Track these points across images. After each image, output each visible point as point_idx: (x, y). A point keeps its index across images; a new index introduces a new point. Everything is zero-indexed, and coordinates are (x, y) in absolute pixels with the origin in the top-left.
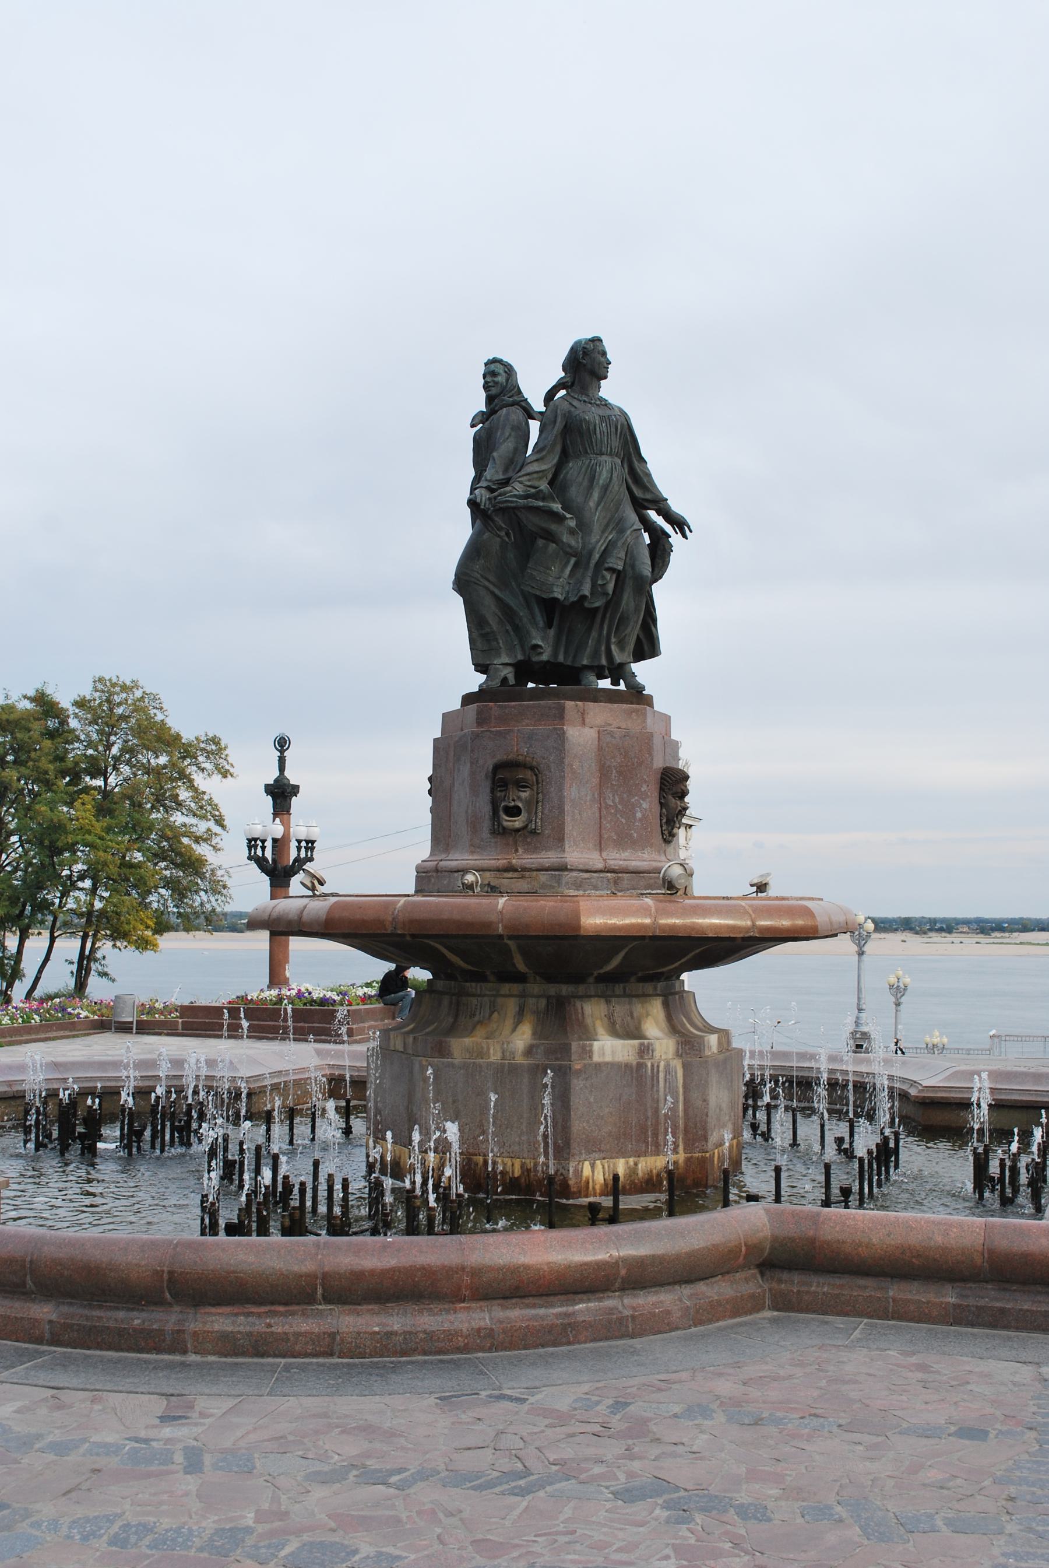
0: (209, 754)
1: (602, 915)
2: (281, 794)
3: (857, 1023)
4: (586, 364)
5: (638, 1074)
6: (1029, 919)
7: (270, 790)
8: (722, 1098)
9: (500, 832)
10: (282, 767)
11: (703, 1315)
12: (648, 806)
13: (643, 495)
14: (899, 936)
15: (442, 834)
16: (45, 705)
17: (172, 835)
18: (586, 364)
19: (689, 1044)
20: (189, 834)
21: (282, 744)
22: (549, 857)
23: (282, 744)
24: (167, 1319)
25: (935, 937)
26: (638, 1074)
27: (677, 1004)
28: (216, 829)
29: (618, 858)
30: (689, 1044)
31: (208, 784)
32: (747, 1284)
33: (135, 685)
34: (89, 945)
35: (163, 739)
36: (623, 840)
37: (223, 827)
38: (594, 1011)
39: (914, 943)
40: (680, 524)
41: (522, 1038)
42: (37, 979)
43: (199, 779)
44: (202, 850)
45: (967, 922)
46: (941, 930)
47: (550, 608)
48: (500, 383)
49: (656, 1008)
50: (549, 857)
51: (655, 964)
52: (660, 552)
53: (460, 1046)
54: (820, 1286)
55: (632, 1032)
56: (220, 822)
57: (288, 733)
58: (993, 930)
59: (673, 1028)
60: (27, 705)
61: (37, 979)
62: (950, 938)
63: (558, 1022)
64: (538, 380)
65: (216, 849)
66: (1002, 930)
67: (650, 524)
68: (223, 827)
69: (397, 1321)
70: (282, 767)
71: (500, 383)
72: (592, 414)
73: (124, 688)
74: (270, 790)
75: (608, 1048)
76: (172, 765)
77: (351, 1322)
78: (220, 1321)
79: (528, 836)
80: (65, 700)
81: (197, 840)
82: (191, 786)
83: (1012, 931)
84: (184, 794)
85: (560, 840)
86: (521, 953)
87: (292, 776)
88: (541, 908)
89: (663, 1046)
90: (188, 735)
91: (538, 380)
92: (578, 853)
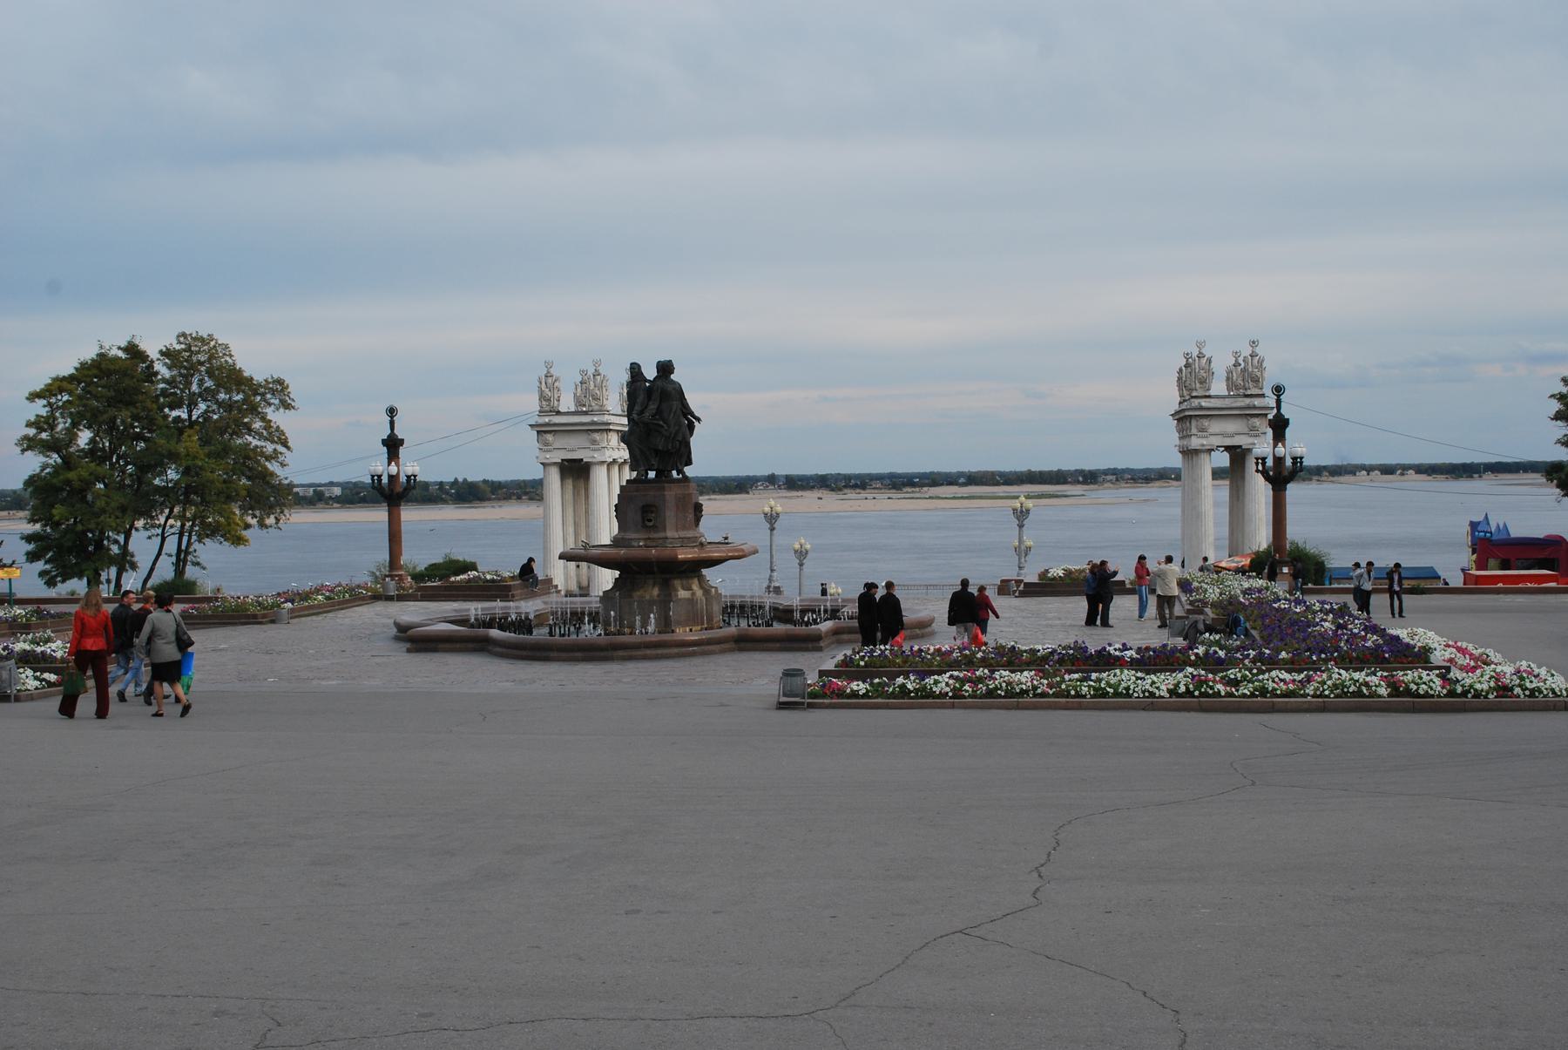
0: (273, 392)
1: (684, 555)
2: (393, 445)
3: (770, 580)
4: (665, 368)
5: (692, 601)
6: (939, 474)
7: (385, 442)
8: (717, 609)
9: (644, 526)
10: (392, 428)
11: (723, 652)
12: (691, 516)
13: (686, 411)
14: (816, 494)
15: (622, 527)
16: (133, 351)
17: (248, 454)
18: (665, 368)
19: (707, 592)
20: (262, 454)
21: (392, 412)
22: (661, 535)
23: (392, 412)
24: (609, 654)
25: (851, 494)
26: (692, 601)
27: (701, 578)
28: (280, 448)
29: (683, 534)
30: (707, 592)
31: (277, 417)
32: (733, 645)
33: (211, 337)
34: (185, 539)
35: (233, 378)
36: (684, 528)
37: (288, 448)
38: (677, 583)
39: (830, 502)
40: (699, 420)
41: (656, 592)
42: (152, 569)
43: (270, 413)
44: (272, 466)
45: (879, 477)
46: (855, 486)
47: (657, 452)
48: (635, 370)
49: (696, 581)
50: (661, 535)
51: (693, 569)
52: (691, 427)
53: (637, 594)
54: (749, 645)
55: (689, 589)
56: (285, 444)
57: (1282, 382)
58: (905, 485)
59: (701, 587)
60: (121, 354)
61: (152, 569)
62: (864, 494)
63: (667, 586)
64: (650, 373)
65: (283, 465)
66: (913, 485)
67: (686, 419)
68: (288, 448)
69: (659, 651)
70: (392, 428)
71: (635, 370)
72: (670, 388)
73: (202, 340)
74: (385, 442)
75: (683, 594)
76: (245, 401)
77: (648, 652)
78: (621, 653)
79: (655, 528)
80: (152, 349)
81: (268, 458)
82: (263, 419)
83: (922, 486)
84: (257, 425)
85: (664, 530)
86: (654, 564)
87: (399, 433)
88: (666, 553)
89: (699, 593)
90: (259, 377)
91: (650, 373)
92: (670, 534)
